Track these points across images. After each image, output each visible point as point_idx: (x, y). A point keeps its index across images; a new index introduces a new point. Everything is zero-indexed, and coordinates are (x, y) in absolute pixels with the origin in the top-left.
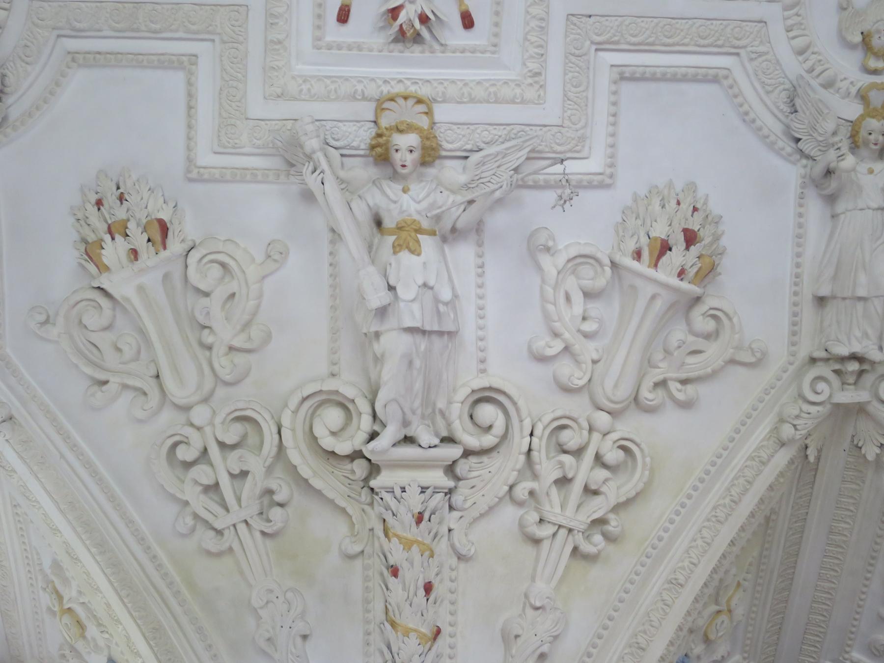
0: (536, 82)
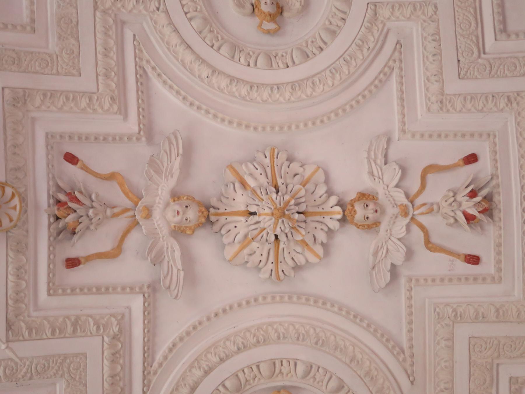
0: (515, 99)
